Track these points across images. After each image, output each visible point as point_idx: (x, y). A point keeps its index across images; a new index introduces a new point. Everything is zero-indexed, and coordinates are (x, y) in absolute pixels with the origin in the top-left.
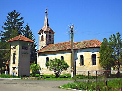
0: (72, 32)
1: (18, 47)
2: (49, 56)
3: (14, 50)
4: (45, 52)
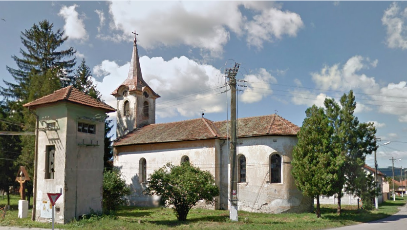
0: (244, 86)
1: (63, 122)
3: (52, 135)
4: (135, 144)
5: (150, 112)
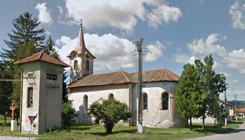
2: (88, 94)
3: (31, 81)
4: (81, 87)
5: (90, 67)
